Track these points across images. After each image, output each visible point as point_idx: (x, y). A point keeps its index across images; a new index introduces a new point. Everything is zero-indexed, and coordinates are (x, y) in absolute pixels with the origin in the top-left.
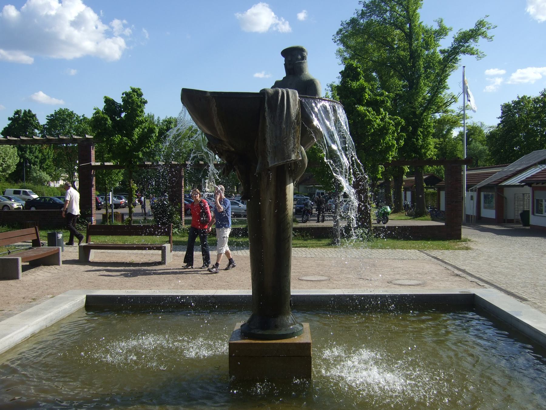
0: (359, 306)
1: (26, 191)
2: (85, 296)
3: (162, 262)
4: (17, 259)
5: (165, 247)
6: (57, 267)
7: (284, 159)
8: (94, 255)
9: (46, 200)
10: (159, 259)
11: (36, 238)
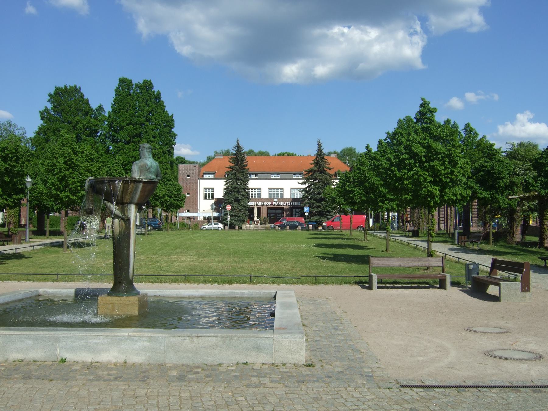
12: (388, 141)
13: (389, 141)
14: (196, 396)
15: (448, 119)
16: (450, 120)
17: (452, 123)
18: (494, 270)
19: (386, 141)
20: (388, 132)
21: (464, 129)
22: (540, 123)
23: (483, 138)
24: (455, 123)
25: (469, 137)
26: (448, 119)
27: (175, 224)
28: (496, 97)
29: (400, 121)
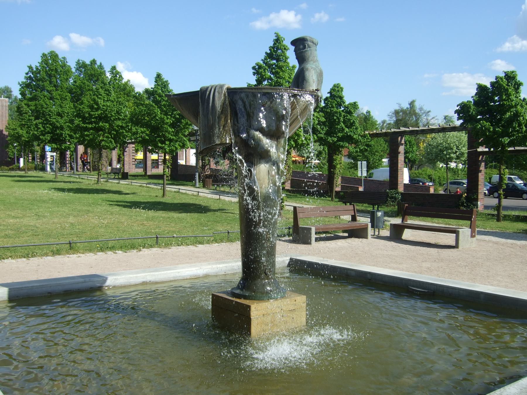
0: (307, 286)
1: (511, 178)
2: (288, 258)
3: (456, 246)
4: (310, 229)
5: (459, 231)
6: (364, 240)
7: (210, 144)
8: (407, 234)
9: (509, 186)
10: (453, 243)
11: (353, 214)
12: (30, 76)
13: (32, 76)
14: (70, 340)
15: (94, 59)
16: (96, 61)
17: (98, 64)
18: (406, 216)
19: (28, 76)
20: (31, 65)
21: (110, 71)
22: (137, 72)
23: (127, 82)
24: (101, 64)
25: (115, 79)
26: (94, 59)
27: (267, 198)
28: (102, 42)
29: (44, 55)
